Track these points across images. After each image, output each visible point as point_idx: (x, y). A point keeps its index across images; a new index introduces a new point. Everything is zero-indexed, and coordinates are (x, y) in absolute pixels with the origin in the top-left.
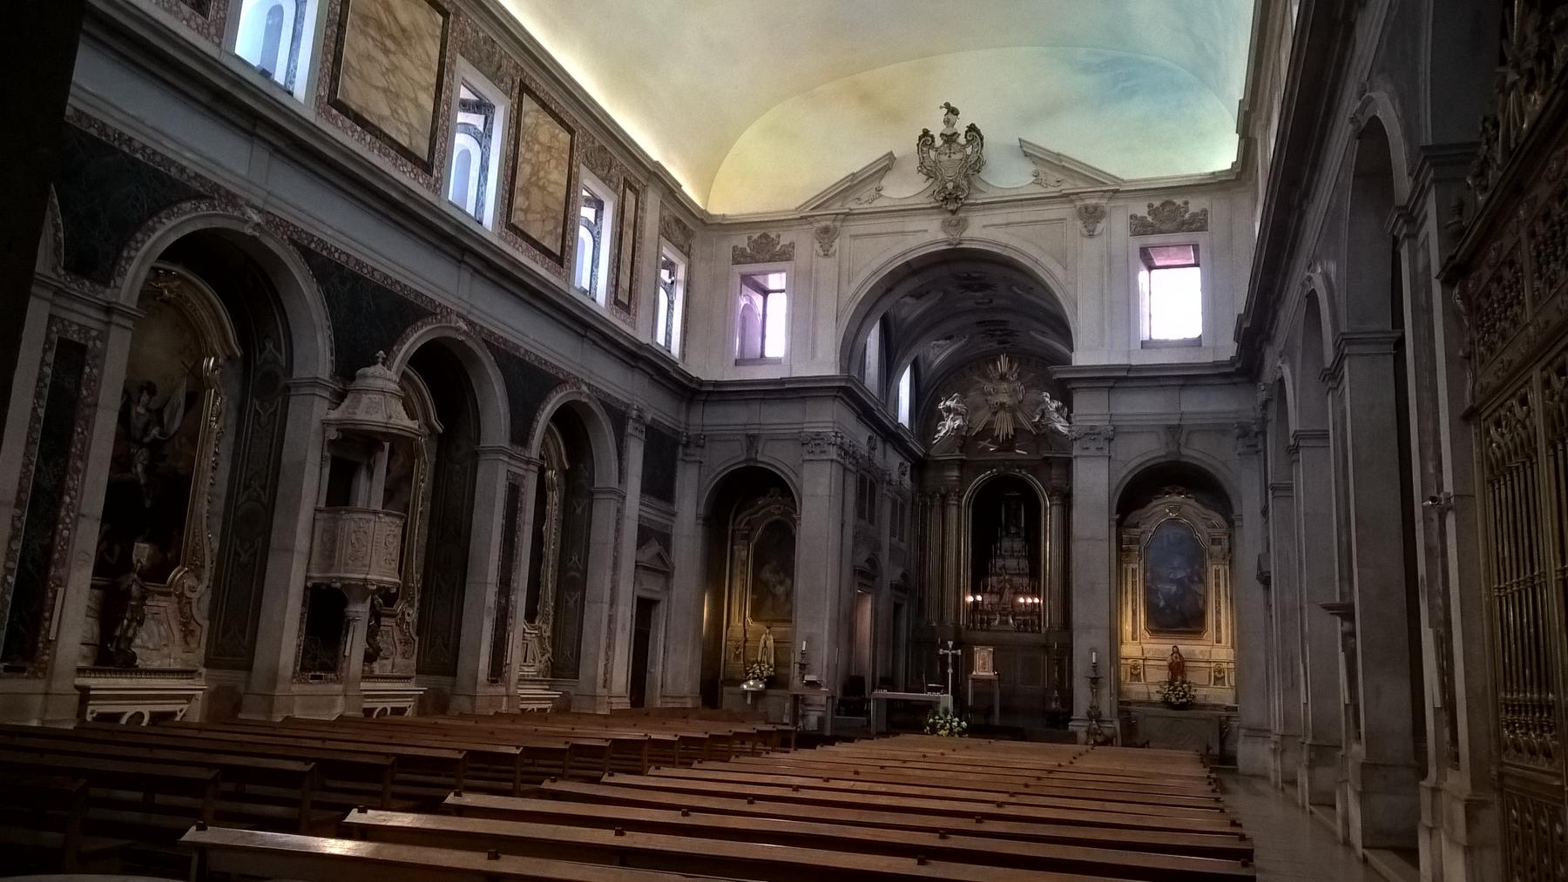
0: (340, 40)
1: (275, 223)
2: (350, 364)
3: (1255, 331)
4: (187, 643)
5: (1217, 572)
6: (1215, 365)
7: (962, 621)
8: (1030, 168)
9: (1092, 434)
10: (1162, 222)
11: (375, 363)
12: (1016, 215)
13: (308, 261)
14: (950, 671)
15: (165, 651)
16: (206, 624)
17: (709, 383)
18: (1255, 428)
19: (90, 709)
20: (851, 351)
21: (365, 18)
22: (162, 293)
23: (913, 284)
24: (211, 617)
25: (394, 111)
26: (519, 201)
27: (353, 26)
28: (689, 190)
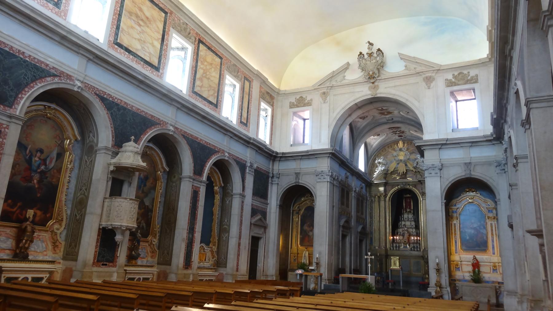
0: (119, 20)
1: (88, 87)
2: (120, 140)
3: (499, 120)
4: (55, 251)
5: (491, 224)
6: (485, 136)
7: (388, 246)
8: (403, 63)
9: (433, 167)
10: (459, 81)
11: (130, 141)
12: (397, 82)
13: (103, 102)
14: (369, 265)
15: (45, 253)
16: (63, 243)
17: (280, 153)
18: (504, 162)
19: (3, 275)
20: (335, 138)
21: (130, 13)
22: (47, 115)
23: (359, 113)
24: (66, 240)
25: (143, 48)
26: (198, 83)
27: (125, 15)
28: (271, 81)
